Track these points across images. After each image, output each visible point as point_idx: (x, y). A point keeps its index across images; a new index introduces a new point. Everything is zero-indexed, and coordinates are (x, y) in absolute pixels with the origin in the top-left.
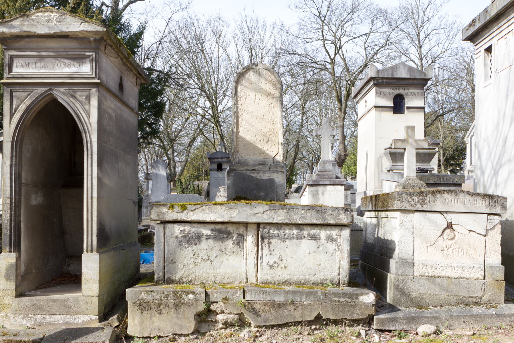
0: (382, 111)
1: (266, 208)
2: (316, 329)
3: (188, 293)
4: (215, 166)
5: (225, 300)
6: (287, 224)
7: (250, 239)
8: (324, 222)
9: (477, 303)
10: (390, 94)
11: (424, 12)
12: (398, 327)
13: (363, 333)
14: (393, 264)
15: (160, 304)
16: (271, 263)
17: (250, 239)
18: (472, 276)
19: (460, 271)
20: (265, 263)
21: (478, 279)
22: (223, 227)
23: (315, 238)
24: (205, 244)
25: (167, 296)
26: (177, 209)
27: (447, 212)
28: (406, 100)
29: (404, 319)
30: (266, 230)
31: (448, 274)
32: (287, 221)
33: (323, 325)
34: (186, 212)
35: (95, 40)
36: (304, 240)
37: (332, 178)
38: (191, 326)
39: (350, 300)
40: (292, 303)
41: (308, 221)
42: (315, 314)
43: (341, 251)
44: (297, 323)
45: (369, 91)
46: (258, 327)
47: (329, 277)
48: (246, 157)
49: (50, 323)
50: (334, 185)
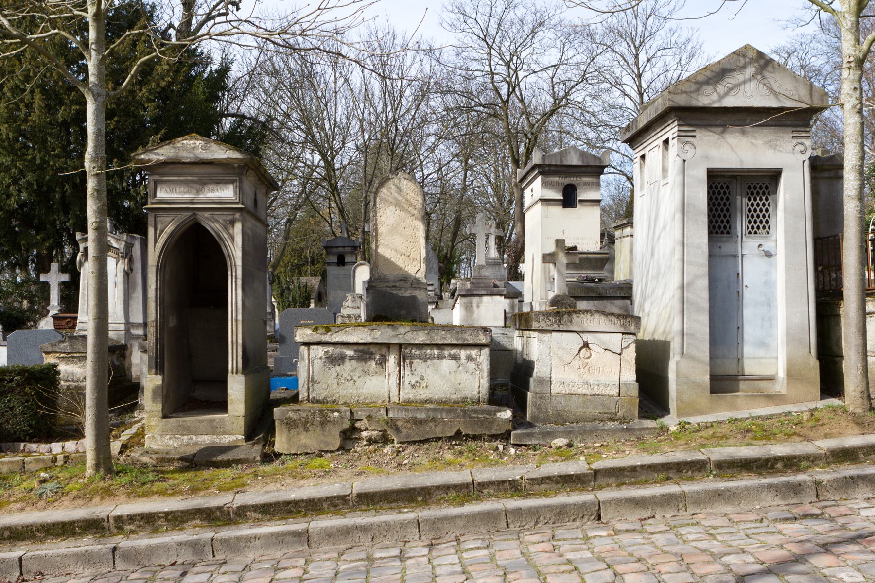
0: (549, 205)
1: (408, 329)
2: (456, 444)
3: (333, 411)
4: (334, 259)
5: (369, 417)
6: (428, 345)
7: (392, 359)
8: (460, 341)
9: (611, 419)
10: (558, 184)
11: (645, 25)
12: (534, 442)
13: (501, 447)
14: (532, 380)
15: (306, 422)
16: (413, 382)
17: (392, 359)
18: (607, 393)
19: (596, 389)
20: (407, 383)
21: (613, 396)
22: (366, 348)
23: (456, 358)
24: (348, 365)
25: (313, 415)
26: (321, 331)
27: (583, 332)
28: (578, 191)
29: (539, 433)
30: (407, 351)
31: (584, 392)
32: (428, 342)
33: (462, 440)
34: (329, 333)
35: (239, 167)
36: (444, 360)
37: (489, 287)
38: (337, 443)
39: (488, 417)
40: (433, 420)
41: (448, 342)
42: (455, 430)
43: (481, 370)
44: (438, 439)
45: (534, 178)
46: (401, 443)
47: (470, 396)
48: (386, 273)
49: (196, 444)
50: (491, 295)
